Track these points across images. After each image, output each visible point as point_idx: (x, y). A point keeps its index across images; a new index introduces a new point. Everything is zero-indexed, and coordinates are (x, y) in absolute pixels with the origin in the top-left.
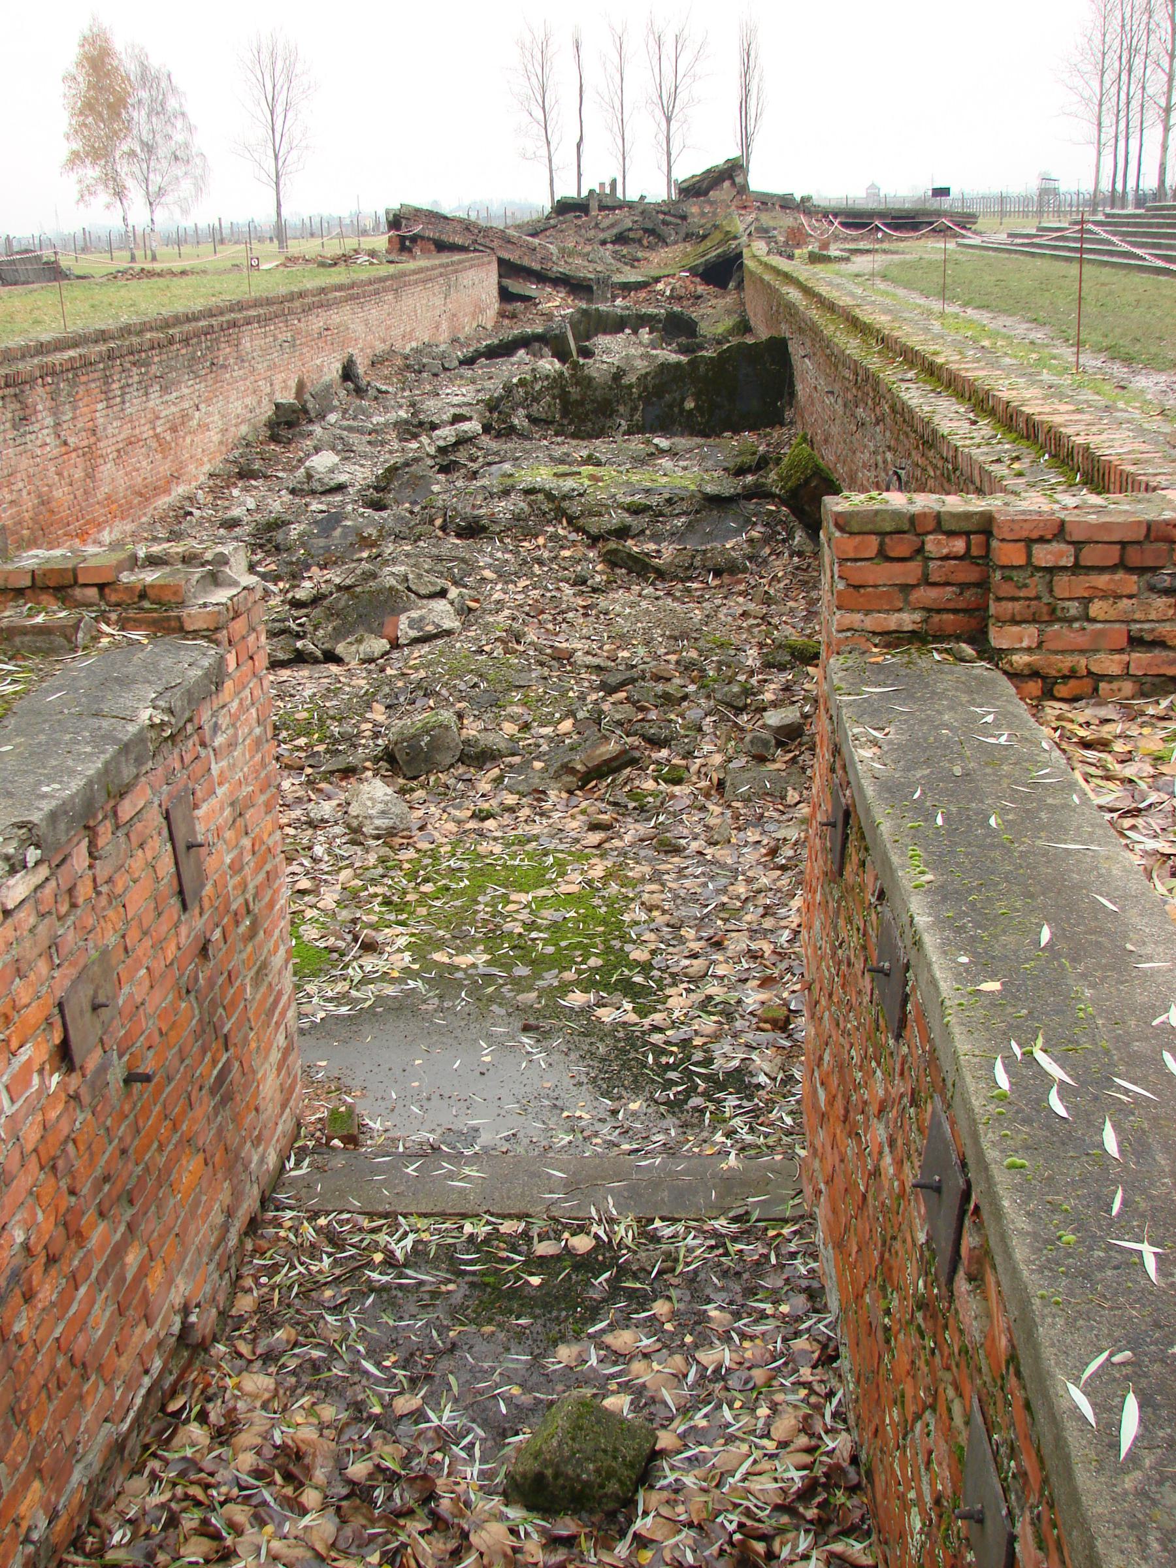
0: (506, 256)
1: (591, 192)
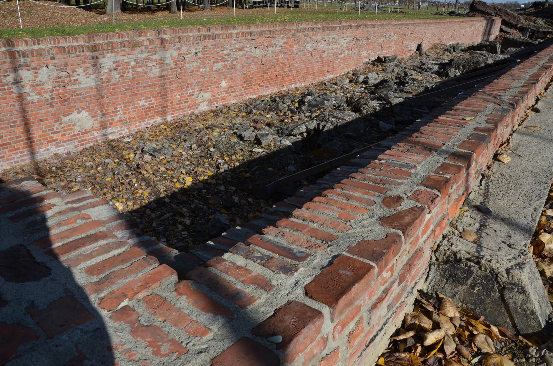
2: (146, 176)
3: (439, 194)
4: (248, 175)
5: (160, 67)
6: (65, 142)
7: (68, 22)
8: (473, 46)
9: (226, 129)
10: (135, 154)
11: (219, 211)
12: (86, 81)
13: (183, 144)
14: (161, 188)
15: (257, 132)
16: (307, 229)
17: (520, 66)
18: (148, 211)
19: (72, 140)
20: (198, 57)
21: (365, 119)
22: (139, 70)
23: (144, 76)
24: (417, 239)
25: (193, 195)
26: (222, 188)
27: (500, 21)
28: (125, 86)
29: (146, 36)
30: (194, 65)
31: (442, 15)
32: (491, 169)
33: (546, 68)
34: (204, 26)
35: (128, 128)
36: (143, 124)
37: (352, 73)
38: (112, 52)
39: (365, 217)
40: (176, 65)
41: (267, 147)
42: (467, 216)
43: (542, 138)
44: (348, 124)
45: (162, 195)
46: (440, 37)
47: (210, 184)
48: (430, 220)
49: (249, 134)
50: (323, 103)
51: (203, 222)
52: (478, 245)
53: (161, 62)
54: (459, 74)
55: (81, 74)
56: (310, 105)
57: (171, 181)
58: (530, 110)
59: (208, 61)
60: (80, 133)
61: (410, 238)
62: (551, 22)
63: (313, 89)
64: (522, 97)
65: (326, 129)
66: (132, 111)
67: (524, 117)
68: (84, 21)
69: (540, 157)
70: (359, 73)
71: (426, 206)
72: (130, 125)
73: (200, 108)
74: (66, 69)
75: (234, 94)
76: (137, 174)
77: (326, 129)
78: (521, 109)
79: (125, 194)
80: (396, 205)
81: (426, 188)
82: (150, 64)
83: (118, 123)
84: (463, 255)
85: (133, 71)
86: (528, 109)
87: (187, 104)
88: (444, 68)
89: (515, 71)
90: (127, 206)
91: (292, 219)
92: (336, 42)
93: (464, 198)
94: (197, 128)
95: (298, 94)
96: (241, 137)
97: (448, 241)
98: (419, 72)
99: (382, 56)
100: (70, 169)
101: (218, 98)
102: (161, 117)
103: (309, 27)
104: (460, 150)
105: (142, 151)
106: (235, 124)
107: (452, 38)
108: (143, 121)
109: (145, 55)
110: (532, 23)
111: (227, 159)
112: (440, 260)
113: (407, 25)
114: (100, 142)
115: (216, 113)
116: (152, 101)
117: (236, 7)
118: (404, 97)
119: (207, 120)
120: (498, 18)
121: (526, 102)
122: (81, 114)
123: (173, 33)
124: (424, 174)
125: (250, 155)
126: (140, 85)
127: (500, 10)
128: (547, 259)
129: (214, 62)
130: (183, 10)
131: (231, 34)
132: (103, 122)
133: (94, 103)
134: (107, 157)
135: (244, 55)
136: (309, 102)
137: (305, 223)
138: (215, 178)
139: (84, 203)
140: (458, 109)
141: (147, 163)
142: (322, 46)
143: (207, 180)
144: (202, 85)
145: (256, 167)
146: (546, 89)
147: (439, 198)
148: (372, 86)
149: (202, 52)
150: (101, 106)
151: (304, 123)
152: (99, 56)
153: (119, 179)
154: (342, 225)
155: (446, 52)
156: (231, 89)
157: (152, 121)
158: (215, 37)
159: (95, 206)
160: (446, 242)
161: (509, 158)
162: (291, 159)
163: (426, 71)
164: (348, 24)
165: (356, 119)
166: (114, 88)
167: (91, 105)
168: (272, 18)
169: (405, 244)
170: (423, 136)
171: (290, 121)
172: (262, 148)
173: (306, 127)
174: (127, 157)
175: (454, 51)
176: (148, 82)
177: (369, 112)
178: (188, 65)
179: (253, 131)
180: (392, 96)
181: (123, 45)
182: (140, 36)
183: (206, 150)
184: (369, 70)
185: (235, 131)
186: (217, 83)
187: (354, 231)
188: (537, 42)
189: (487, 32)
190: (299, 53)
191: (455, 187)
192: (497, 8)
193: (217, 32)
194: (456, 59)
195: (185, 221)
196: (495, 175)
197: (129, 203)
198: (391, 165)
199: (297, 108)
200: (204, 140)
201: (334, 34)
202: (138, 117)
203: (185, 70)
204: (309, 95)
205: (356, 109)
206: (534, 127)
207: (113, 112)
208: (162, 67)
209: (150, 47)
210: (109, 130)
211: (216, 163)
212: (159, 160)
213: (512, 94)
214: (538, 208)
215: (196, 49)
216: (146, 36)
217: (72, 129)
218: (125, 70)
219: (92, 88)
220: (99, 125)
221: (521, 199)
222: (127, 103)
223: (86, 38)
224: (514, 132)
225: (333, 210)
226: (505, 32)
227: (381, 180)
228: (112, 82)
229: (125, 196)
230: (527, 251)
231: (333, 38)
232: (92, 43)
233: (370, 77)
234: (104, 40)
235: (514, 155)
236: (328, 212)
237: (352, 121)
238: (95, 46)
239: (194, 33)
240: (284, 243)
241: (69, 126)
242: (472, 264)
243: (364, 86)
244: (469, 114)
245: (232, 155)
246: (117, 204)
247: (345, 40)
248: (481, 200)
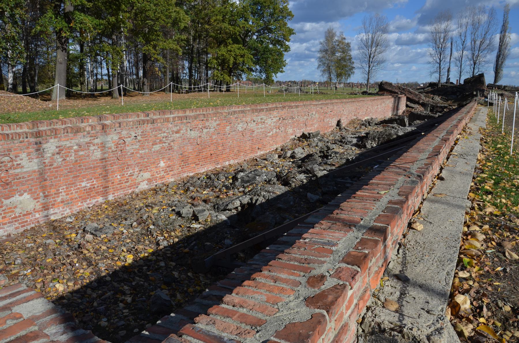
2: (88, 255)
3: (359, 270)
4: (187, 250)
5: (101, 150)
6: (5, 224)
7: (13, 109)
8: (385, 120)
9: (165, 207)
10: (77, 233)
11: (160, 287)
12: (29, 164)
13: (124, 222)
14: (102, 267)
15: (194, 209)
16: (237, 315)
17: (424, 139)
18: (89, 291)
19: (13, 222)
20: (137, 140)
21: (294, 192)
22: (81, 153)
23: (86, 159)
24: (342, 314)
25: (134, 272)
26: (162, 264)
27: (405, 98)
28: (67, 169)
29: (88, 122)
30: (134, 147)
31: (356, 94)
32: (407, 237)
33: (446, 141)
34: (143, 112)
35: (70, 209)
36: (85, 204)
37: (280, 149)
38: (55, 138)
39: (291, 298)
40: (117, 148)
41: (204, 223)
42: (388, 286)
43: (448, 204)
44: (279, 197)
45: (103, 274)
46: (356, 113)
47: (150, 261)
48: (352, 295)
49: (187, 211)
50: (254, 178)
51: (144, 299)
52: (400, 314)
53: (103, 146)
54: (375, 145)
55: (24, 159)
56: (243, 181)
57: (112, 259)
58: (436, 179)
59: (147, 144)
60: (21, 215)
61: (335, 316)
62: (445, 99)
63: (245, 166)
64: (427, 169)
65: (258, 202)
66: (74, 192)
67: (432, 185)
68: (29, 108)
69: (448, 223)
70: (286, 148)
71: (348, 284)
72: (72, 205)
73: (140, 187)
74: (9, 154)
75: (172, 173)
76: (78, 253)
77: (258, 202)
78: (428, 179)
79: (66, 274)
80: (320, 284)
81: (347, 265)
82: (92, 148)
83: (61, 204)
84: (386, 325)
85: (76, 154)
86: (435, 178)
87: (127, 184)
88: (361, 141)
89: (421, 144)
90: (68, 286)
91: (223, 306)
93: (383, 269)
94: (137, 206)
95: (232, 170)
96: (179, 214)
97: (372, 312)
98: (341, 145)
99: (306, 133)
100: (9, 251)
101: (157, 177)
102: (102, 197)
103: (239, 110)
104: (376, 224)
105: (84, 230)
106: (173, 201)
107: (366, 114)
108: (85, 202)
109: (87, 139)
110: (431, 100)
111: (166, 235)
112: (366, 331)
113: (327, 104)
114: (41, 223)
115: (155, 191)
116: (93, 182)
117: (173, 92)
118: (328, 169)
119: (146, 198)
120: (403, 95)
121: (432, 172)
122: (23, 196)
123: (114, 119)
124: (345, 251)
125: (189, 231)
126: (82, 167)
127: (403, 89)
128: (464, 320)
129: (153, 145)
130: (125, 95)
131: (168, 118)
132: (45, 203)
133: (36, 185)
134: (48, 238)
135: (181, 137)
136: (242, 178)
137: (235, 309)
138: (156, 254)
139: (18, 297)
140: (373, 184)
141: (88, 242)
142: (252, 126)
143: (148, 257)
144: (141, 165)
145: (194, 242)
146: (448, 158)
147: (359, 274)
148: (299, 160)
149: (141, 135)
150: (44, 188)
151: (238, 198)
152: (43, 142)
153: (60, 260)
154: (270, 308)
155: (363, 126)
156: (169, 168)
157: (94, 201)
158: (153, 122)
159: (29, 301)
160: (370, 313)
161: (422, 225)
162: (226, 233)
163: (346, 144)
164: (274, 106)
165: (286, 192)
166: (57, 171)
167: (33, 188)
168: (206, 102)
169: (330, 322)
170: (343, 212)
171: (225, 197)
172: (200, 223)
173: (240, 201)
174: (69, 237)
175: (369, 125)
176: (90, 164)
177: (297, 185)
178: (128, 148)
179: (190, 208)
180: (318, 169)
181: (66, 131)
182: (82, 122)
183: (146, 228)
184: (296, 146)
185: (174, 208)
186: (155, 163)
187: (281, 314)
188: (437, 116)
189: (396, 108)
190: (231, 133)
191: (374, 260)
192: (402, 87)
193: (155, 117)
194: (371, 133)
195: (126, 298)
196: (410, 243)
197: (69, 284)
198: (315, 243)
199: (231, 184)
200: (144, 218)
201: (262, 115)
202: (80, 197)
203: (125, 152)
204: (242, 172)
205: (285, 182)
206: (440, 194)
207: (55, 194)
208: (103, 150)
209: (92, 132)
210: (51, 211)
211: (156, 239)
212: (100, 239)
213: (419, 166)
214: (450, 272)
215: (136, 133)
216: (88, 122)
217: (13, 211)
218: (67, 154)
219: (35, 171)
220: (41, 206)
221: (435, 265)
222: (69, 184)
223: (30, 125)
224: (424, 200)
225: (261, 293)
226: (410, 107)
227: (306, 259)
228: (55, 165)
229: (66, 277)
230: (444, 316)
231: (261, 119)
232: (35, 130)
233: (296, 152)
234: (47, 126)
235: (425, 222)
236: (256, 296)
237: (282, 195)
238: (39, 132)
239: (133, 118)
240: (215, 332)
241: (10, 208)
242: (396, 333)
243: (292, 160)
244: (383, 188)
245: (171, 231)
246: (57, 286)
248: (399, 268)
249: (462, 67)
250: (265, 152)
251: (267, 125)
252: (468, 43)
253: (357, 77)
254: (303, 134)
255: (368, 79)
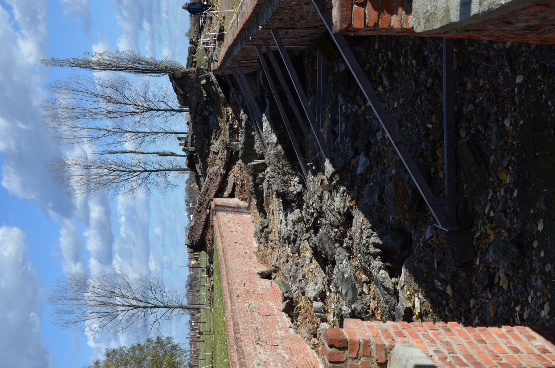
0: (213, 193)
1: (184, 150)
65: (378, 241)
77: (378, 241)
92: (265, 362)
99: (283, 306)
127: (201, 204)
175: (267, 227)
233: (315, 293)
247: (260, 353)
249: (155, 130)
250: (320, 363)
251: (270, 359)
252: (109, 124)
253: (177, 330)
254: (285, 311)
255: (181, 307)
